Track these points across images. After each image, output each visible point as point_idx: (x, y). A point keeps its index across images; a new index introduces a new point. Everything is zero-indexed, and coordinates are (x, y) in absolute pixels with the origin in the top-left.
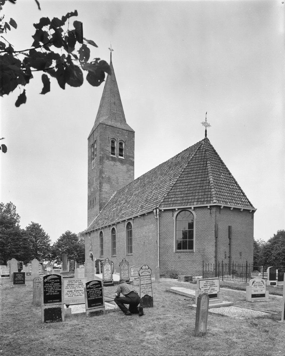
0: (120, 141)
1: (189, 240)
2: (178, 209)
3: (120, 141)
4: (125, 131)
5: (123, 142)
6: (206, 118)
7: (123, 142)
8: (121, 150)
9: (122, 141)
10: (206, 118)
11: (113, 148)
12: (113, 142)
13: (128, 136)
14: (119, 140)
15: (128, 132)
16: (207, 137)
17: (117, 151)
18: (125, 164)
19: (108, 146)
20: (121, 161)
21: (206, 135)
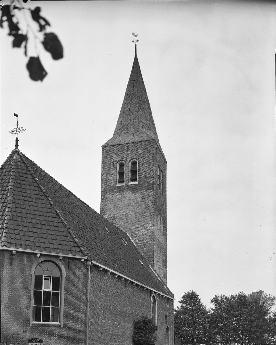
0: (132, 161)
1: (42, 304)
2: (42, 255)
3: (132, 161)
4: (139, 144)
5: (123, 162)
6: (18, 122)
7: (123, 162)
8: (134, 172)
9: (134, 159)
10: (18, 122)
11: (121, 174)
12: (122, 165)
14: (128, 160)
15: (143, 143)
16: (19, 148)
17: (127, 175)
18: (138, 191)
20: (133, 189)
21: (17, 146)
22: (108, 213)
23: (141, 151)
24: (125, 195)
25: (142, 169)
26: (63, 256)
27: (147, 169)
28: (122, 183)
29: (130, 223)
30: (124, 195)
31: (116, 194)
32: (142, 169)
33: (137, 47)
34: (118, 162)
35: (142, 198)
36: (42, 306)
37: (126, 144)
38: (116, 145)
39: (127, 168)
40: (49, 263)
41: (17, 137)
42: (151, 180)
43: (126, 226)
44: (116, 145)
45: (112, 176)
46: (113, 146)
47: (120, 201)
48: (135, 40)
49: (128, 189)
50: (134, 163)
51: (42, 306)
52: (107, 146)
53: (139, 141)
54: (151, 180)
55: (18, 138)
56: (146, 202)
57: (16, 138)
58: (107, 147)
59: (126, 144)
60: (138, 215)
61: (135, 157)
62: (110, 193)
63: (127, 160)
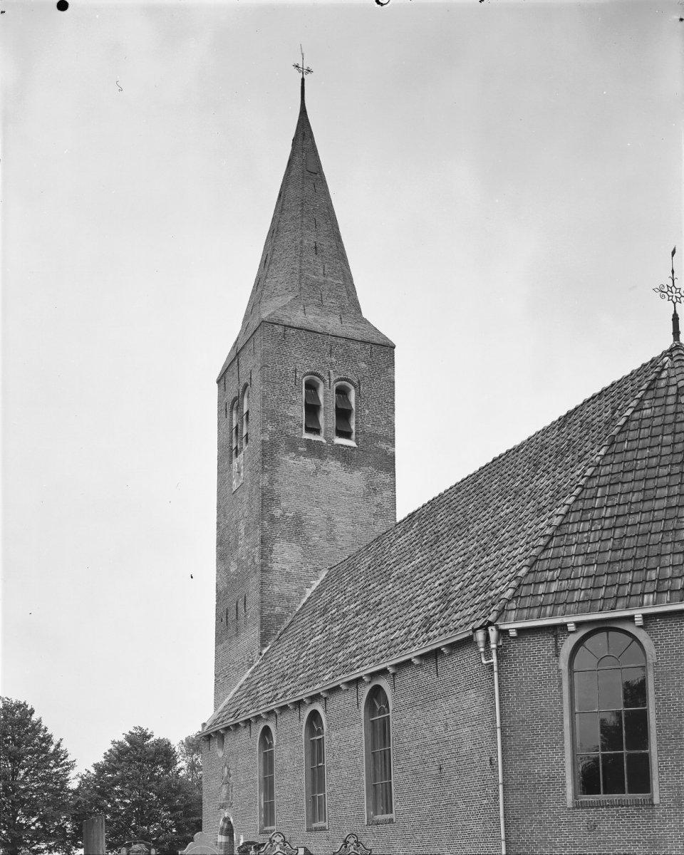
0: (339, 383)
2: (579, 625)
3: (339, 383)
4: (358, 346)
6: (673, 272)
8: (343, 414)
10: (673, 272)
11: (312, 409)
12: (311, 387)
13: (369, 363)
14: (333, 378)
15: (368, 347)
17: (327, 419)
19: (294, 403)
20: (345, 456)
21: (676, 333)
22: (284, 504)
23: (363, 365)
24: (326, 469)
25: (367, 411)
26: (574, 622)
27: (378, 416)
28: (315, 434)
29: (339, 543)
30: (323, 468)
31: (302, 458)
32: (367, 411)
33: (305, 86)
34: (305, 375)
35: (368, 486)
36: (625, 751)
37: (328, 335)
38: (302, 329)
39: (326, 397)
40: (587, 643)
41: (675, 311)
42: (388, 447)
43: (332, 549)
44: (302, 329)
45: (292, 408)
46: (293, 327)
47: (312, 479)
48: (301, 66)
49: (333, 455)
50: (342, 392)
51: (625, 751)
52: (277, 324)
53: (360, 339)
54: (388, 447)
55: (677, 312)
56: (378, 499)
57: (673, 313)
58: (276, 326)
59: (328, 335)
60: (359, 529)
61: (350, 375)
62: (287, 452)
63: (330, 379)
